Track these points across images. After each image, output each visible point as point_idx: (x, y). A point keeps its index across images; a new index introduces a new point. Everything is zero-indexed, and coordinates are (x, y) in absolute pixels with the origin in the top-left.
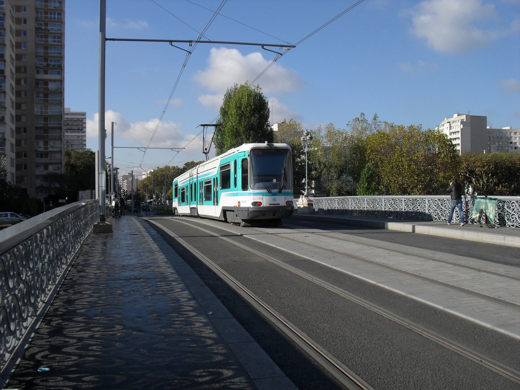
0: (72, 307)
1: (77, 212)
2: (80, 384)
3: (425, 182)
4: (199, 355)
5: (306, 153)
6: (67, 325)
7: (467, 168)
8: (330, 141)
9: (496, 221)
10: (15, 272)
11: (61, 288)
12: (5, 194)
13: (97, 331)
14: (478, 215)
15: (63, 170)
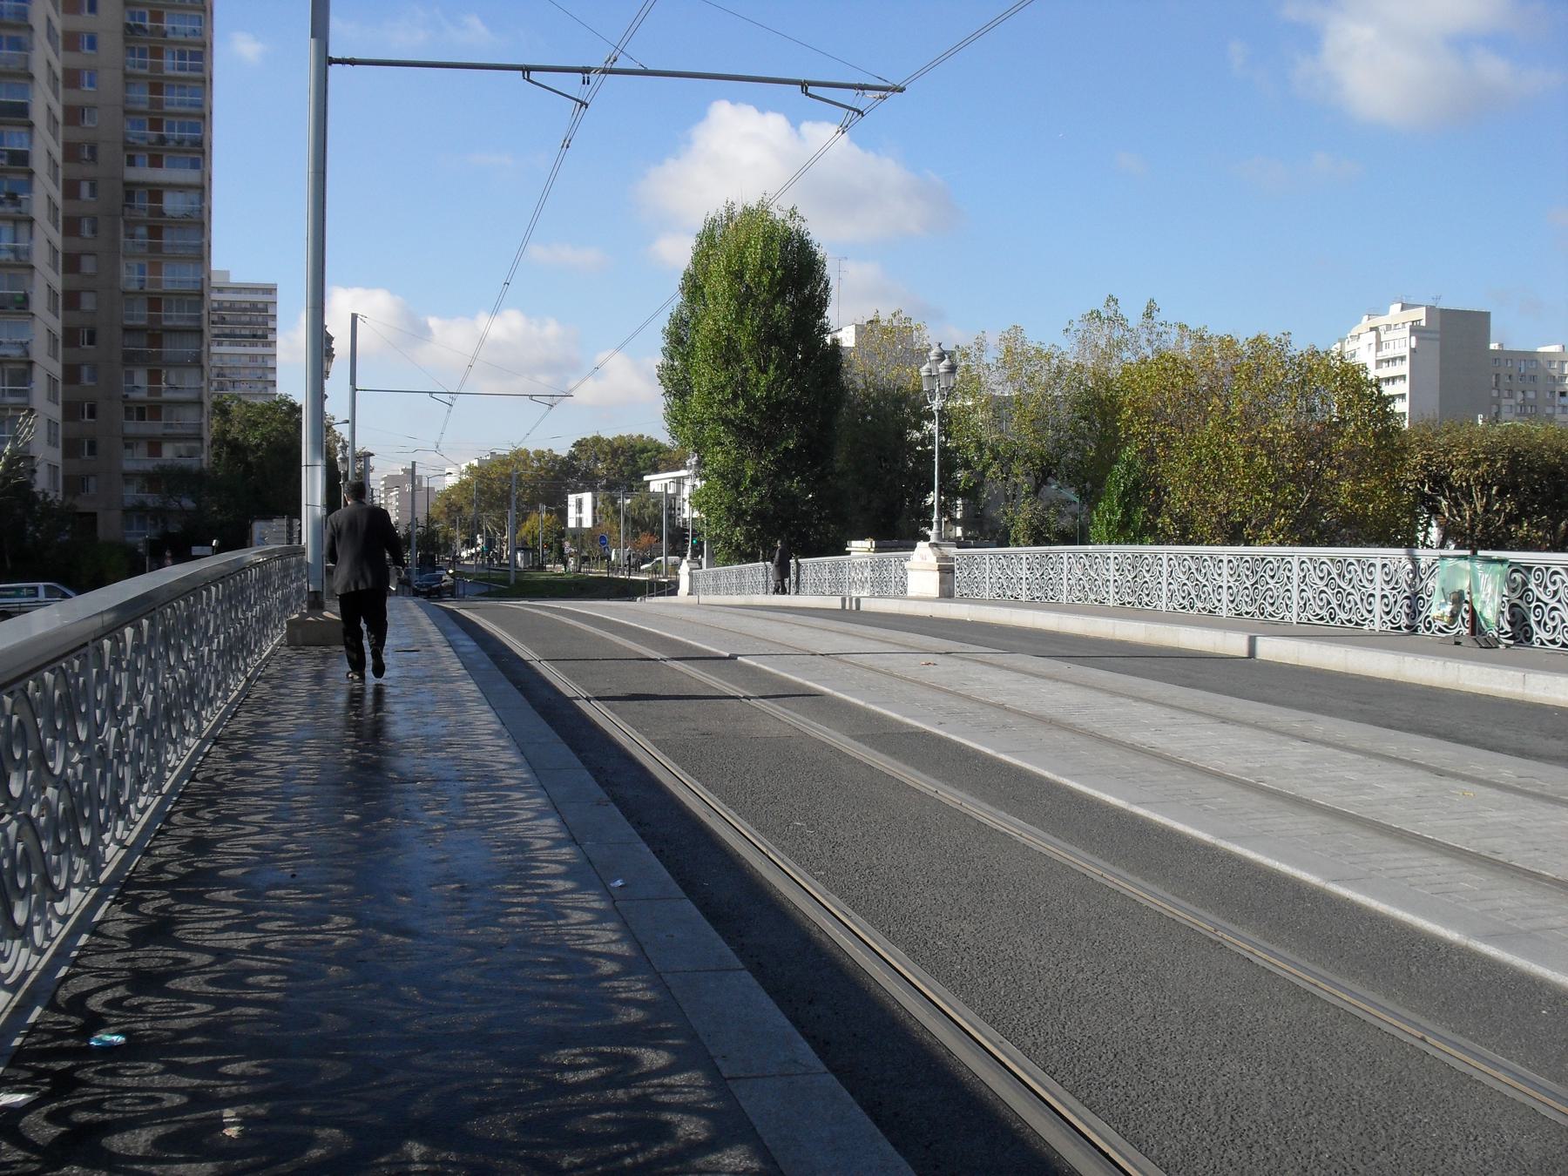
0: (205, 861)
1: (235, 580)
2: (212, 1082)
3: (1298, 507)
4: (572, 1007)
5: (936, 414)
6: (187, 911)
7: (1424, 468)
8: (1011, 379)
9: (1502, 629)
10: (30, 752)
11: (177, 803)
12: (31, 528)
13: (275, 931)
14: (1448, 608)
15: (206, 459)
